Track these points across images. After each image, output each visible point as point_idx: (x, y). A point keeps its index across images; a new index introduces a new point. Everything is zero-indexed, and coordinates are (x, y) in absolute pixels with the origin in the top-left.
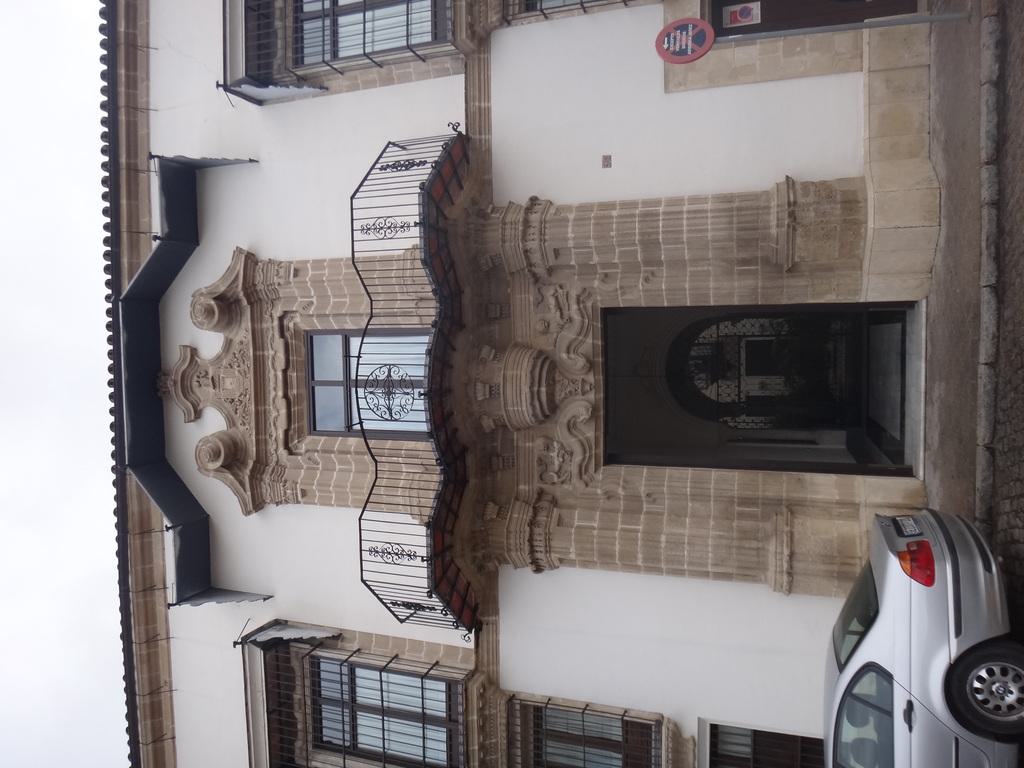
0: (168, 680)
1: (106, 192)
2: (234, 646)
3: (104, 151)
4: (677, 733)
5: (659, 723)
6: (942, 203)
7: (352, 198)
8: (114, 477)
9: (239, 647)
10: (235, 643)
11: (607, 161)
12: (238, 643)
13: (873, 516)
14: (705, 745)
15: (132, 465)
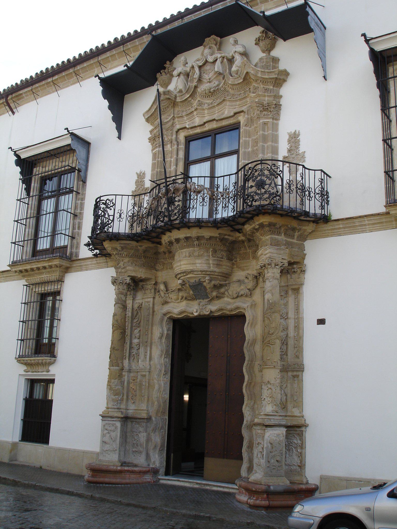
0: (108, 68)
1: (118, 39)
2: (65, 129)
3: (109, 42)
4: (50, 364)
5: (55, 356)
6: (125, 501)
7: (322, 171)
8: (183, 11)
9: (66, 132)
10: (67, 129)
11: (321, 322)
12: (68, 131)
13: (294, 409)
14: (42, 377)
15: (154, 37)
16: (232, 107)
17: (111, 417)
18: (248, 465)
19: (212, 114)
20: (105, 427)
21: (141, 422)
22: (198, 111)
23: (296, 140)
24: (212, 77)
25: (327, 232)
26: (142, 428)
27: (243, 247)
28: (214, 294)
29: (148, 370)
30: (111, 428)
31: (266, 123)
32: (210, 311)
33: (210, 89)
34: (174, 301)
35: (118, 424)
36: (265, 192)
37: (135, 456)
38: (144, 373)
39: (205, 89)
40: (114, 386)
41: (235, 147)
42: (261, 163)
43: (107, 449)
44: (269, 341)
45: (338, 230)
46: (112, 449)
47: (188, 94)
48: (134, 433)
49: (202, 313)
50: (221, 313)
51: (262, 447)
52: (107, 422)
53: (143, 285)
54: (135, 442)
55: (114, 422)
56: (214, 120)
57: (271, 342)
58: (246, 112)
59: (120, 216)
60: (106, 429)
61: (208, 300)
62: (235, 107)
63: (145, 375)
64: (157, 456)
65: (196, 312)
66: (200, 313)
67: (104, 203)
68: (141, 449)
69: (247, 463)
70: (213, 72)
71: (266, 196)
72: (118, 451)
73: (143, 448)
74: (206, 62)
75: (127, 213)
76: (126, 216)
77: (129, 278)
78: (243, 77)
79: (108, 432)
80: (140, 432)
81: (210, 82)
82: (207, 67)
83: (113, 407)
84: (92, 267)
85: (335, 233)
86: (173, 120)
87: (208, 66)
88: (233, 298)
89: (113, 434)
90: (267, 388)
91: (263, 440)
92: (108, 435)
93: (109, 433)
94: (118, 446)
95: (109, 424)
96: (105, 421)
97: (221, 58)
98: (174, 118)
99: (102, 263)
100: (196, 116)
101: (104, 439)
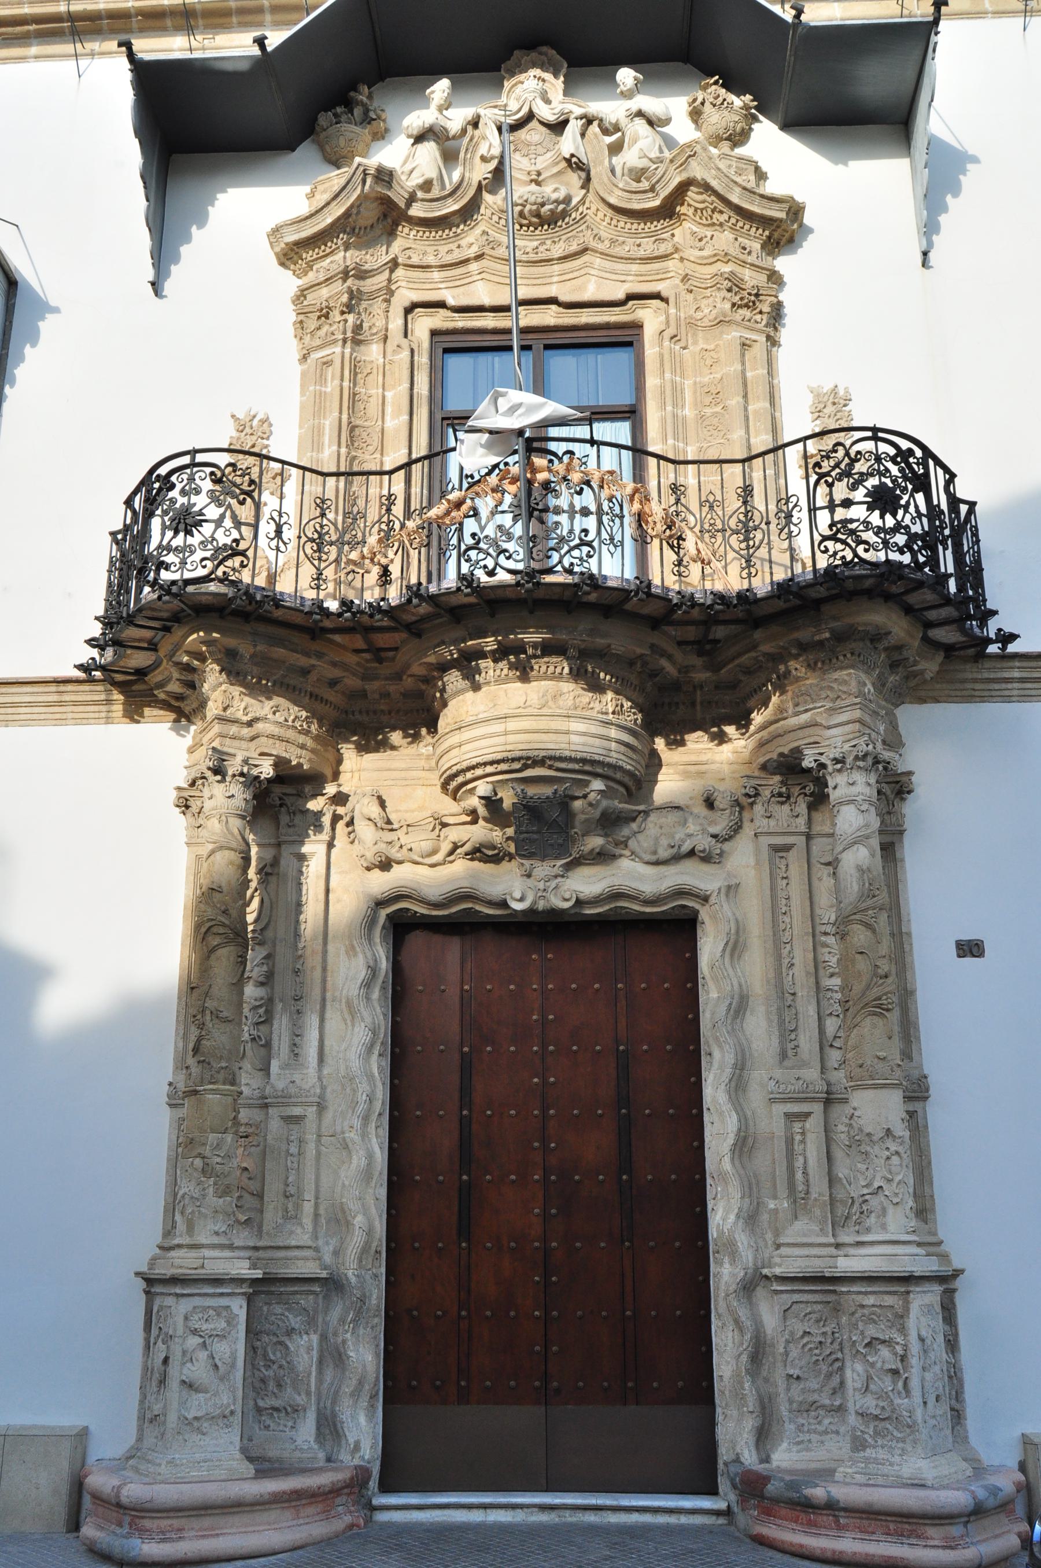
11: (970, 949)
16: (614, 277)
17: (217, 1281)
18: (758, 1422)
19: (538, 281)
20: (190, 1324)
21: (296, 1293)
22: (484, 263)
23: (838, 411)
24: (546, 168)
25: (969, 686)
26: (296, 1316)
27: (684, 704)
28: (596, 842)
29: (317, 1099)
30: (212, 1326)
31: (748, 342)
32: (574, 900)
33: (543, 205)
34: (420, 860)
35: (239, 1308)
36: (897, 528)
37: (267, 1427)
38: (297, 1111)
39: (526, 201)
40: (219, 1160)
41: (624, 398)
42: (875, 438)
43: (199, 1414)
44: (880, 999)
45: (1004, 686)
46: (218, 1411)
47: (456, 201)
48: (265, 1339)
49: (541, 905)
50: (607, 908)
51: (901, 1352)
52: (198, 1301)
53: (285, 794)
54: (270, 1373)
55: (223, 1302)
56: (553, 301)
57: (885, 1002)
58: (672, 301)
59: (279, 532)
60: (195, 1332)
61: (568, 860)
62: (623, 278)
63: (298, 1120)
64: (362, 1419)
65: (522, 899)
66: (534, 902)
67: (215, 475)
68: (297, 1397)
69: (754, 1415)
70: (549, 155)
71: (901, 539)
72: (237, 1419)
73: (308, 1394)
74: (530, 116)
75: (302, 530)
76: (299, 537)
77: (271, 762)
78: (665, 193)
79: (201, 1340)
80: (290, 1332)
81: (538, 183)
82: (534, 134)
83: (216, 1240)
84: (35, 717)
85: (994, 693)
86: (392, 271)
87: (532, 132)
88: (657, 863)
89: (222, 1348)
90: (888, 1153)
91: (903, 1330)
92: (203, 1355)
93: (204, 1345)
94: (240, 1393)
95: (205, 1309)
96: (191, 1298)
97: (581, 119)
98: (394, 264)
99: (95, 703)
100: (479, 277)
101: (185, 1371)
